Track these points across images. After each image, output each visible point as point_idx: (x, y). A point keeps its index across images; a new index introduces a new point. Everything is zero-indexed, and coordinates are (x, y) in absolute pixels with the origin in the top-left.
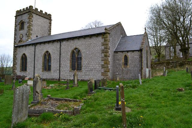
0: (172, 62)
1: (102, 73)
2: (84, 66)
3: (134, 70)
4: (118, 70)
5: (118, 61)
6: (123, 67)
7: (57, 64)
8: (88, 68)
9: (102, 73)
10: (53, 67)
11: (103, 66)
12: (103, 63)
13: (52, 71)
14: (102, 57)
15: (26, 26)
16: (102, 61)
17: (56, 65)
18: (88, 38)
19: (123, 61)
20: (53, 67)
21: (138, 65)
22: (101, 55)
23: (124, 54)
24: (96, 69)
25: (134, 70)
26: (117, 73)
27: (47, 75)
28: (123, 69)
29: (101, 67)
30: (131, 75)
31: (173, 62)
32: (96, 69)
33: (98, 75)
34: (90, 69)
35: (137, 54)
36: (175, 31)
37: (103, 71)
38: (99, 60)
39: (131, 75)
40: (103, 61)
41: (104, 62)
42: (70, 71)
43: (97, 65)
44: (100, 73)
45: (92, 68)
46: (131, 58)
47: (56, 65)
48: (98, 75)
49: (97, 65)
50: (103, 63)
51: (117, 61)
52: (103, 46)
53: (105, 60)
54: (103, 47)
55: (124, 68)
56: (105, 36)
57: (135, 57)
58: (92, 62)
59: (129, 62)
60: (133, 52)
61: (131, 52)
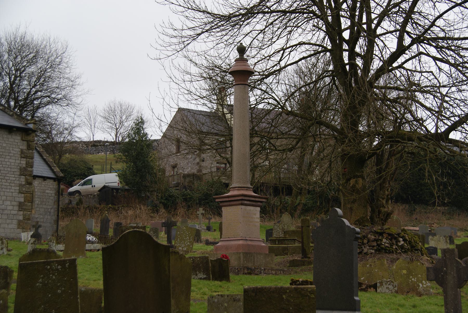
3: (45, 219)
11: (21, 206)
12: (22, 200)
14: (20, 185)
16: (20, 192)
18: (259, 287)
21: (52, 211)
22: (17, 179)
24: (6, 212)
25: (45, 219)
29: (16, 208)
32: (6, 212)
33: (10, 226)
35: (52, 187)
37: (21, 218)
38: (13, 191)
40: (23, 195)
41: (25, 198)
43: (8, 203)
44: (15, 222)
46: (39, 194)
48: (10, 226)
49: (8, 203)
50: (22, 200)
52: (25, 159)
54: (24, 162)
56: (30, 138)
57: (47, 191)
60: (44, 180)
61: (40, 180)
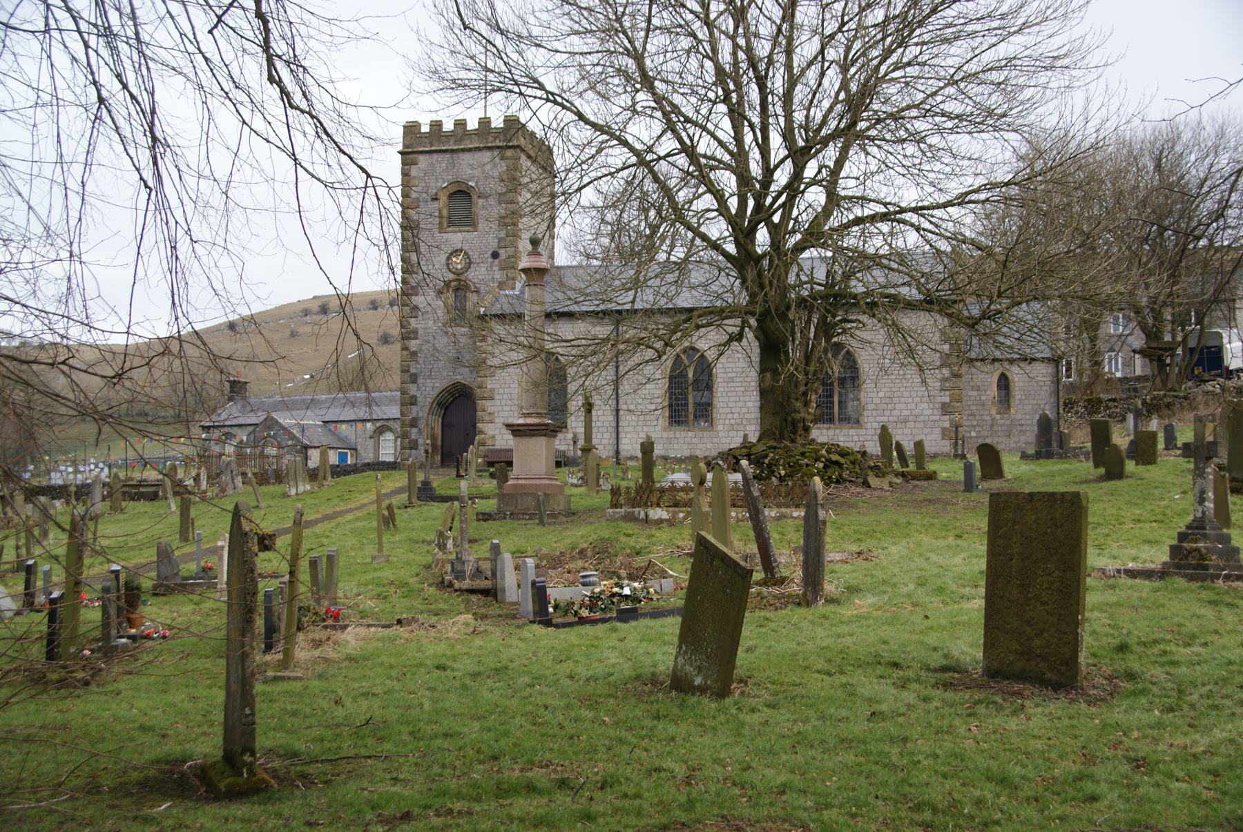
0: (1110, 400)
1: (944, 430)
2: (871, 406)
4: (975, 423)
5: (975, 393)
6: (994, 412)
7: (747, 398)
8: (887, 413)
9: (944, 430)
10: (728, 410)
12: (947, 400)
13: (720, 428)
15: (487, 210)
17: (741, 404)
19: (993, 391)
20: (728, 410)
23: (998, 369)
24: (922, 418)
26: (973, 434)
27: (695, 440)
28: (993, 419)
30: (1023, 438)
31: (1114, 400)
32: (922, 418)
34: (895, 419)
36: (734, 101)
39: (1023, 438)
41: (951, 396)
42: (665, 430)
43: (925, 406)
44: (937, 431)
45: (905, 413)
47: (741, 404)
51: (971, 393)
53: (953, 388)
55: (998, 417)
58: (906, 394)
59: (1017, 394)
